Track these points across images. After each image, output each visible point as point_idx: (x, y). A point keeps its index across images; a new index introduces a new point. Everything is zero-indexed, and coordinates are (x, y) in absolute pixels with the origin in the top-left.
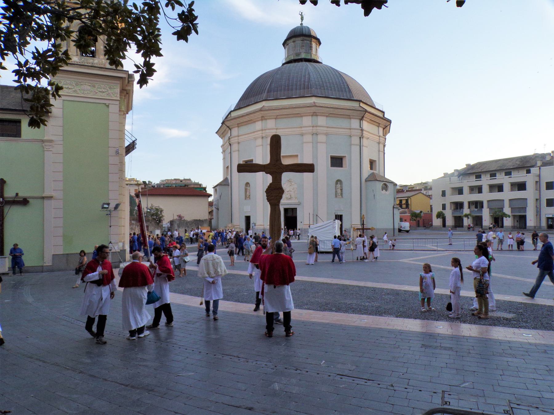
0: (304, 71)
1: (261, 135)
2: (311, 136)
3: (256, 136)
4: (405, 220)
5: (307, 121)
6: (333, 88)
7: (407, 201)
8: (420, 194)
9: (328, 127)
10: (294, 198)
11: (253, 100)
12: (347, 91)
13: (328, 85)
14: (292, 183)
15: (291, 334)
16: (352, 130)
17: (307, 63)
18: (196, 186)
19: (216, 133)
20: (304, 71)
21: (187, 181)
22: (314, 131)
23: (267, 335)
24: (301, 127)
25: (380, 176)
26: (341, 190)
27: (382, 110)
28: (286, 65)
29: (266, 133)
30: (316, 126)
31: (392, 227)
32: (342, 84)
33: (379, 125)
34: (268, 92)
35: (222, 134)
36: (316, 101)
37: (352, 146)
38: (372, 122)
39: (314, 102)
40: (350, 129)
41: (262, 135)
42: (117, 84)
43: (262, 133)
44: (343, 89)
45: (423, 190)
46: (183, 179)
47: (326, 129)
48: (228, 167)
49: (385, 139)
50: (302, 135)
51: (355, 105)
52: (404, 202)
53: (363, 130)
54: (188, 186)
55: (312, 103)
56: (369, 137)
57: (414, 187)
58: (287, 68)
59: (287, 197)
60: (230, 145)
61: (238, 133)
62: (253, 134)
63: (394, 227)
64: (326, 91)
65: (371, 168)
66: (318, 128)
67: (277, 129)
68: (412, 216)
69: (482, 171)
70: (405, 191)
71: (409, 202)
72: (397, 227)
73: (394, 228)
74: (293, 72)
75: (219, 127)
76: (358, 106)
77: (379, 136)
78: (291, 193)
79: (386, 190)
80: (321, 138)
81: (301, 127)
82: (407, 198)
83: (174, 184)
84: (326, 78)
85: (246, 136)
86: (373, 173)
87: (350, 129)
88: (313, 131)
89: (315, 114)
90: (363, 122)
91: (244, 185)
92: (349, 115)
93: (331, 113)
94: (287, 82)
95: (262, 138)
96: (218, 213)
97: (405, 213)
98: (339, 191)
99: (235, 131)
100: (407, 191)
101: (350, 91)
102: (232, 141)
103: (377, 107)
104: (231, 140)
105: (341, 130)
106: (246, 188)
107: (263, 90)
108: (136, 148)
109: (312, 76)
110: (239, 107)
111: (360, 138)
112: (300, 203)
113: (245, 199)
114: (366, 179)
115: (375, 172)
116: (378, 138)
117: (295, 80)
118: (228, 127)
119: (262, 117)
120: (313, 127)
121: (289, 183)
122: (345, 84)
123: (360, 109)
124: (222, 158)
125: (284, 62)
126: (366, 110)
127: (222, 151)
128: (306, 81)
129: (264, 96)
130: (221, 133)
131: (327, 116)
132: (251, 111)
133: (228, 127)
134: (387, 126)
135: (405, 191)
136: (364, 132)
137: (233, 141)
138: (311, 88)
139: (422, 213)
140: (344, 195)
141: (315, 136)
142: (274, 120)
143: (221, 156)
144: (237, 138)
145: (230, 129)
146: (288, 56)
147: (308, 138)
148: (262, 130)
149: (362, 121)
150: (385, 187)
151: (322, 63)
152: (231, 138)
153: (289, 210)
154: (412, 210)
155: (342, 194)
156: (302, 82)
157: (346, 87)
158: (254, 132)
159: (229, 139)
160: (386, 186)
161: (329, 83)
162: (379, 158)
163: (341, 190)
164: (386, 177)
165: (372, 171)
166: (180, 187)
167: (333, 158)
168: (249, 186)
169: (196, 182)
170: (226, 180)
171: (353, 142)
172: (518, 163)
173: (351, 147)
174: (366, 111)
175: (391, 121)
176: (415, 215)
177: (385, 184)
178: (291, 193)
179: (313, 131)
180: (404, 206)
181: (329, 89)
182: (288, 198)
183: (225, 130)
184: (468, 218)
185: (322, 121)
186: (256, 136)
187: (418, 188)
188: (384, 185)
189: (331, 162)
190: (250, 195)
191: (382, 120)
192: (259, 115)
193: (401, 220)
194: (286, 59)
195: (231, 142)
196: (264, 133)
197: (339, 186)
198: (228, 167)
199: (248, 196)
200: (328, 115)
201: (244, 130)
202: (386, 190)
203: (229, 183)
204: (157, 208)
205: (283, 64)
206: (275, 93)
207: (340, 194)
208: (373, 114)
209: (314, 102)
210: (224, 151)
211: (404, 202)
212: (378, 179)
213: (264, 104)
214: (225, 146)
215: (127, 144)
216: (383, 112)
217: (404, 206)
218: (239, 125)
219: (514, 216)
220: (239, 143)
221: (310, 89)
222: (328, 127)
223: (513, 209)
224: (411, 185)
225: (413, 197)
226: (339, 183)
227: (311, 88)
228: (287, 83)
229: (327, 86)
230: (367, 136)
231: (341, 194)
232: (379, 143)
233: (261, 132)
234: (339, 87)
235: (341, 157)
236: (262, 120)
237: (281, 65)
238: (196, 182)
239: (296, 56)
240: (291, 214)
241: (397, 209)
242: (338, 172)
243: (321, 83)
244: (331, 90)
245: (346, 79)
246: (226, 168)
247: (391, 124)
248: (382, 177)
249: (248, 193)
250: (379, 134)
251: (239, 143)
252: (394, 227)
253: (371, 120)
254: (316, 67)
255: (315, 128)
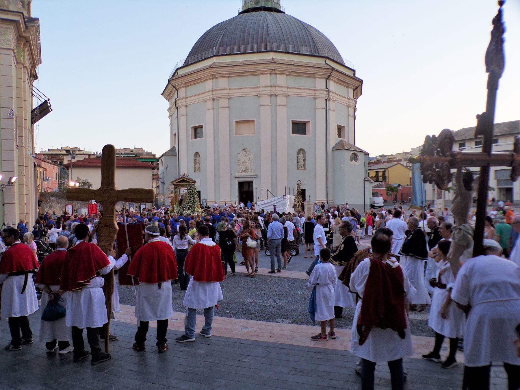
0: (261, 21)
1: (212, 96)
2: (269, 98)
3: (206, 97)
4: (381, 195)
5: (265, 80)
6: (294, 41)
7: (384, 172)
8: (399, 165)
9: (288, 88)
10: (250, 170)
11: (202, 56)
12: (311, 45)
13: (289, 38)
14: (248, 153)
15: (165, 349)
16: (316, 92)
17: (266, 12)
18: (148, 157)
19: (162, 94)
20: (261, 21)
21: (138, 151)
22: (273, 92)
23: (138, 348)
24: (258, 87)
25: (349, 144)
26: (304, 160)
27: (352, 68)
28: (242, 14)
29: (217, 94)
30: (275, 87)
31: (363, 203)
32: (305, 38)
33: (348, 86)
34: (220, 46)
35: (169, 95)
36: (274, 57)
37: (317, 109)
38: (340, 82)
39: (272, 58)
40: (314, 90)
41: (213, 97)
42: (9, 28)
43: (213, 95)
44: (307, 43)
45: (403, 160)
46: (134, 148)
47: (286, 89)
48: (175, 134)
49: (356, 102)
50: (259, 96)
51: (320, 62)
52: (380, 174)
53: (330, 91)
54: (139, 156)
55: (270, 59)
56: (336, 99)
57: (395, 158)
58: (243, 18)
59: (242, 168)
60: (177, 108)
61: (186, 94)
62: (203, 96)
63: (365, 202)
64: (287, 45)
65: (340, 135)
66: (277, 89)
67: (230, 89)
68: (388, 190)
69: (467, 138)
70: (383, 162)
71: (386, 175)
72: (368, 202)
73: (365, 204)
74: (249, 23)
75: (165, 88)
76: (324, 63)
77: (349, 99)
78: (246, 164)
79: (356, 161)
80: (281, 100)
81: (258, 87)
82: (383, 170)
83: (123, 154)
84: (291, 31)
85: (195, 98)
86: (341, 141)
87: (314, 90)
88: (272, 92)
89: (273, 72)
90: (329, 82)
91: (193, 156)
92: (349, 84)
93: (292, 72)
94: (242, 34)
95: (213, 100)
96: (164, 187)
97: (381, 186)
98: (302, 162)
99: (182, 92)
100: (385, 162)
101: (315, 45)
102: (179, 103)
103: (346, 65)
104: (178, 102)
105: (303, 91)
106: (195, 158)
107: (214, 44)
108: (52, 110)
109: (271, 28)
110: (186, 65)
111: (326, 100)
112: (257, 176)
113: (195, 171)
114: (334, 147)
115: (343, 139)
116: (348, 100)
117: (251, 33)
118: (174, 87)
119: (212, 75)
120: (271, 87)
121: (244, 152)
122: (309, 38)
123: (326, 66)
124: (169, 124)
125: (241, 10)
126: (332, 67)
127: (169, 116)
128: (264, 33)
129: (216, 51)
130: (167, 93)
131: (287, 75)
132: (200, 68)
133: (174, 87)
134: (357, 87)
135: (383, 162)
136: (331, 94)
137: (180, 104)
138: (269, 42)
139: (401, 186)
140: (307, 166)
141: (273, 98)
142: (227, 78)
143: (168, 121)
144: (184, 100)
145: (177, 90)
146: (245, 4)
147: (266, 100)
148: (213, 91)
149: (329, 80)
150: (354, 157)
151: (284, 13)
152: (178, 100)
153: (245, 184)
154: (389, 183)
155: (304, 165)
156: (260, 35)
157: (310, 40)
158: (203, 93)
159: (176, 101)
160: (356, 156)
161: (291, 36)
162: (348, 124)
163: (304, 160)
164: (356, 145)
165: (340, 139)
166: (129, 157)
167: (294, 123)
168: (199, 157)
169: (148, 152)
170: (173, 149)
171: (317, 106)
172: (506, 129)
173: (315, 111)
174: (333, 69)
175: (362, 81)
176: (391, 188)
177: (355, 154)
178: (246, 164)
179: (272, 92)
180: (381, 179)
181: (291, 42)
182: (243, 170)
183: (171, 91)
184: (449, 192)
185: (281, 80)
186: (206, 97)
187: (398, 159)
188: (353, 155)
189: (293, 129)
190: (199, 167)
191: (351, 80)
192: (209, 72)
193: (375, 194)
194: (243, 8)
195: (178, 105)
196: (216, 94)
197: (301, 156)
198: (175, 134)
199: (197, 168)
200: (291, 74)
201: (193, 90)
202: (356, 161)
203: (176, 153)
204: (84, 181)
205: (240, 14)
206: (228, 47)
207: (302, 166)
208: (341, 73)
209: (272, 58)
210: (171, 116)
211: (380, 174)
212: (346, 148)
213: (215, 60)
214: (172, 109)
215: (36, 103)
216: (354, 71)
217: (381, 179)
218: (186, 85)
219: (500, 189)
220: (186, 106)
221: (268, 43)
222: (288, 88)
223: (499, 181)
224: (392, 155)
225: (391, 168)
226: (301, 152)
227: (269, 42)
228: (242, 36)
229: (288, 40)
230: (334, 98)
231: (304, 165)
232: (348, 107)
233: (211, 93)
234: (302, 41)
235: (305, 123)
236: (212, 79)
237: (238, 14)
238: (148, 152)
239: (254, 4)
240: (247, 189)
241: (369, 182)
242: (300, 140)
243: (281, 36)
244: (293, 44)
245: (312, 31)
246: (173, 135)
247: (363, 84)
248: (352, 145)
249: (197, 164)
250: (348, 96)
251: (186, 106)
252: (365, 202)
253: (339, 79)
254: (276, 17)
255: (274, 89)
